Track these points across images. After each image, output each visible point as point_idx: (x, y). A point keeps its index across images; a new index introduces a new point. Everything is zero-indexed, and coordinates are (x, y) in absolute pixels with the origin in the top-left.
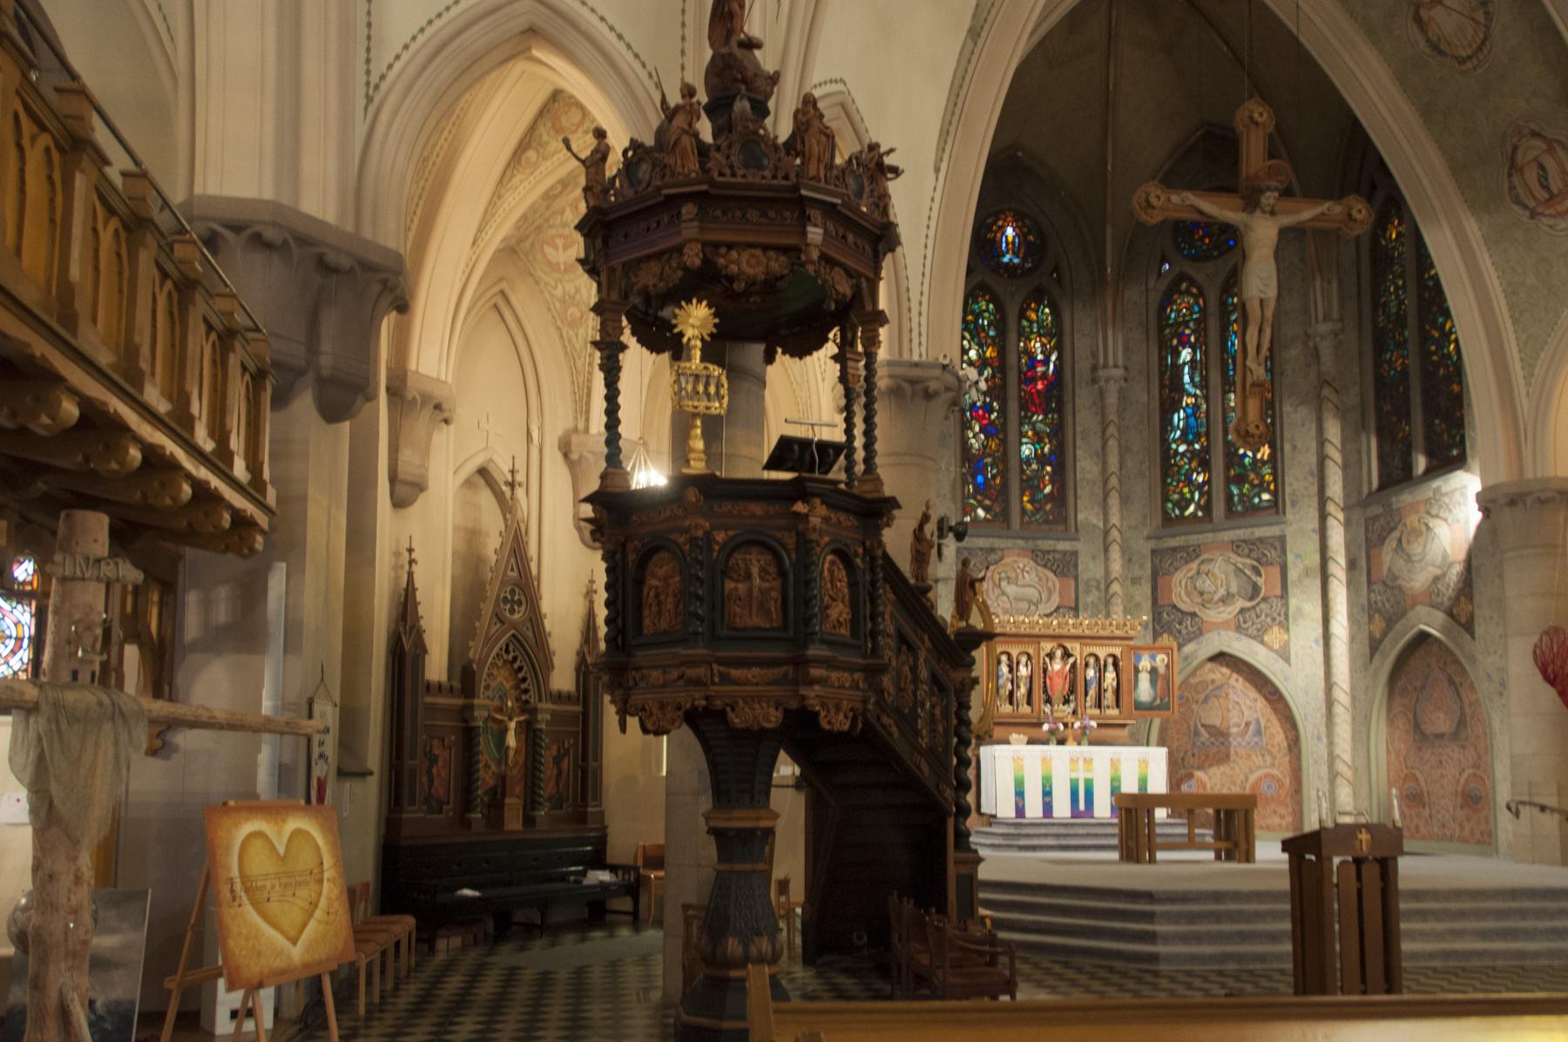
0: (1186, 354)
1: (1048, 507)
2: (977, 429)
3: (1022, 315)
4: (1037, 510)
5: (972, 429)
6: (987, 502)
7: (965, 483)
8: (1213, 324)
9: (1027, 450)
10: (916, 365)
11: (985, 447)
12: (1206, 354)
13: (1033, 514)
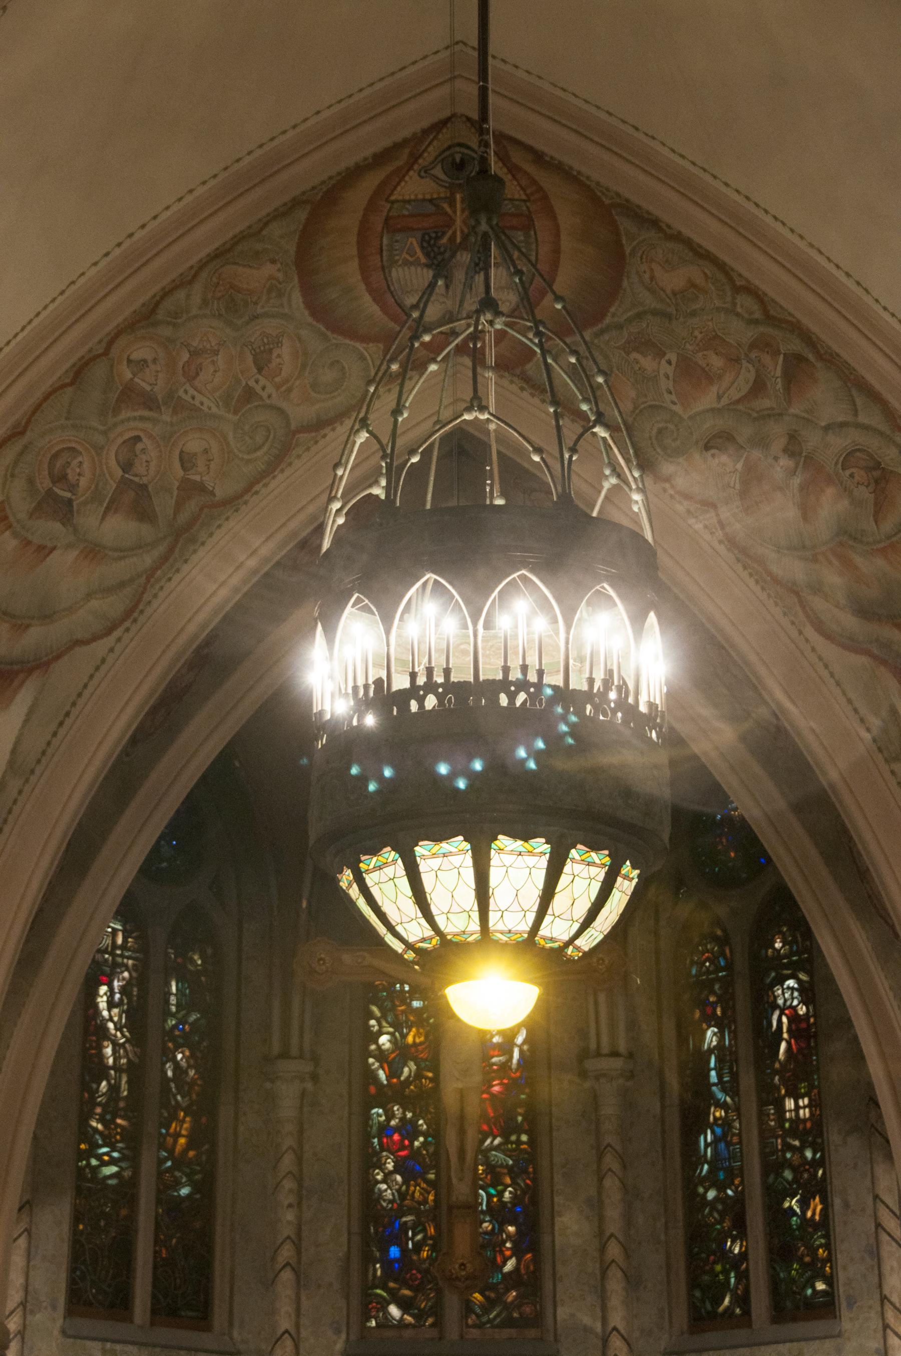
0: (711, 1036)
2: (390, 1166)
4: (490, 1304)
5: (381, 1166)
7: (367, 1260)
8: (742, 991)
11: (402, 1195)
12: (734, 1036)
13: (486, 1310)
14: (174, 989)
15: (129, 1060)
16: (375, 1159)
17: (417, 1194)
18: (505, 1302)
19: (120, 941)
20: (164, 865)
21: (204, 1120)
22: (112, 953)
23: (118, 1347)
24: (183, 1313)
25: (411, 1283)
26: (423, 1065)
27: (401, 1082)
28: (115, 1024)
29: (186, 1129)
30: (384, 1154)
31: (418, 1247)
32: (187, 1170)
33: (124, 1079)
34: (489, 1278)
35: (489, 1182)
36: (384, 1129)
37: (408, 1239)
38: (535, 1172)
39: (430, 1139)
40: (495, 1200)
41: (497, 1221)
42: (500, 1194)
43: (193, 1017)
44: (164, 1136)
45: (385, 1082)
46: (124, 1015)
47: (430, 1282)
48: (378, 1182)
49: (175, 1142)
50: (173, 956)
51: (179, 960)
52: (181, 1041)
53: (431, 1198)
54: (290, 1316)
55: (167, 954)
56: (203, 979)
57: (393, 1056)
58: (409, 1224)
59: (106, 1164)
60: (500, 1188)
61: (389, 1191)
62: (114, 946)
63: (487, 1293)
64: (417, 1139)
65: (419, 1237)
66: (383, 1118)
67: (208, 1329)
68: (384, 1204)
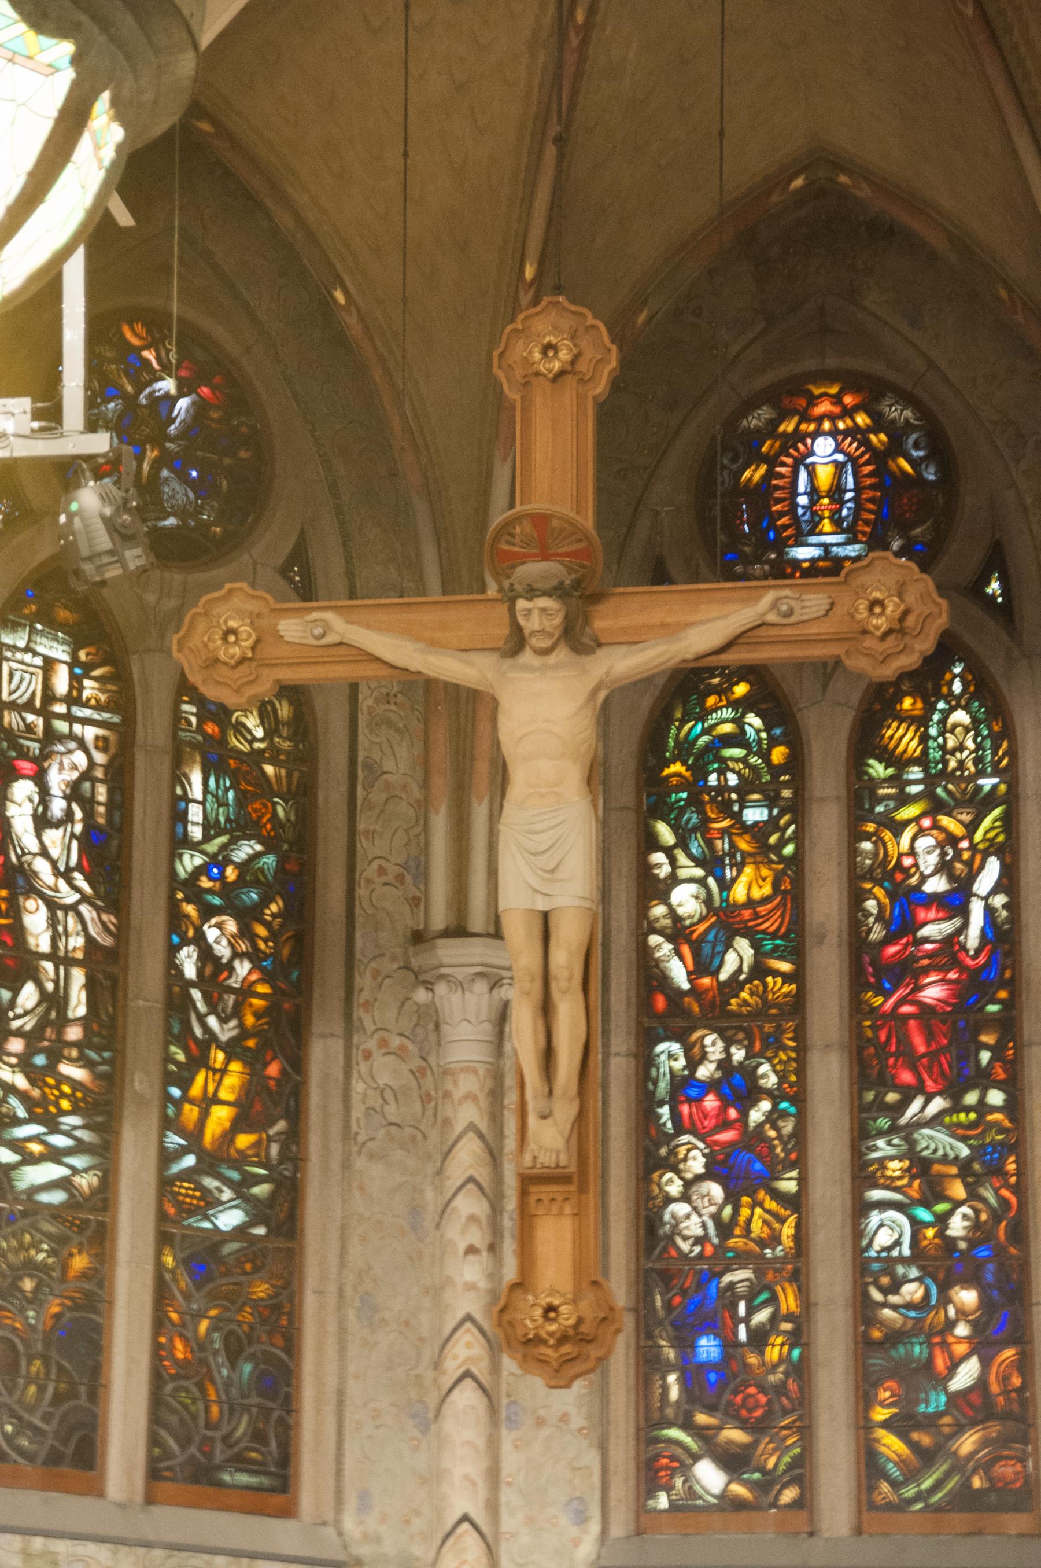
1: (967, 1443)
2: (696, 1164)
3: (866, 741)
6: (734, 1435)
9: (888, 1230)
11: (725, 1229)
13: (912, 1475)
14: (196, 791)
15: (90, 940)
16: (663, 1151)
17: (756, 1226)
18: (955, 1454)
19: (61, 683)
20: (171, 521)
21: (273, 1070)
22: (48, 716)
23: (61, 1547)
24: (227, 1478)
25: (744, 1413)
26: (768, 946)
27: (722, 986)
28: (54, 863)
29: (232, 1088)
30: (685, 1138)
31: (759, 1338)
32: (235, 1175)
33: (78, 976)
34: (918, 1402)
35: (916, 1195)
36: (684, 1086)
37: (736, 1321)
38: (1020, 1173)
39: (784, 1105)
40: (930, 1233)
41: (935, 1280)
42: (943, 1220)
43: (244, 851)
44: (178, 1104)
45: (686, 986)
46: (75, 844)
47: (785, 1412)
48: (669, 1200)
49: (205, 1114)
50: (194, 720)
51: (211, 728)
52: (217, 901)
53: (788, 1230)
54: (474, 1484)
55: (177, 717)
56: (269, 769)
57: (701, 928)
58: (741, 1289)
59: (30, 1159)
60: (941, 1207)
61: (695, 1218)
62: (49, 696)
63: (915, 1436)
64: (754, 1103)
65: (762, 1316)
66: (682, 1062)
67: (288, 1511)
68: (685, 1246)
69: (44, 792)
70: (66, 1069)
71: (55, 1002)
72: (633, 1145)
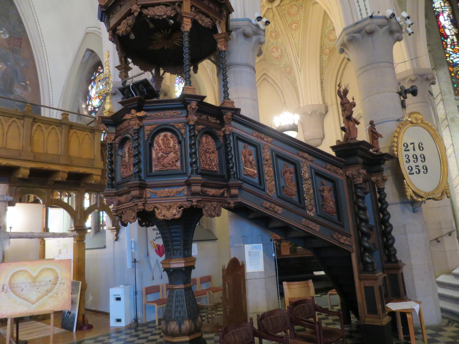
10: (357, 23)
19: (442, 4)
59: (455, 58)
69: (444, 18)
70: (456, 48)
71: (452, 40)
72: (449, 175)
